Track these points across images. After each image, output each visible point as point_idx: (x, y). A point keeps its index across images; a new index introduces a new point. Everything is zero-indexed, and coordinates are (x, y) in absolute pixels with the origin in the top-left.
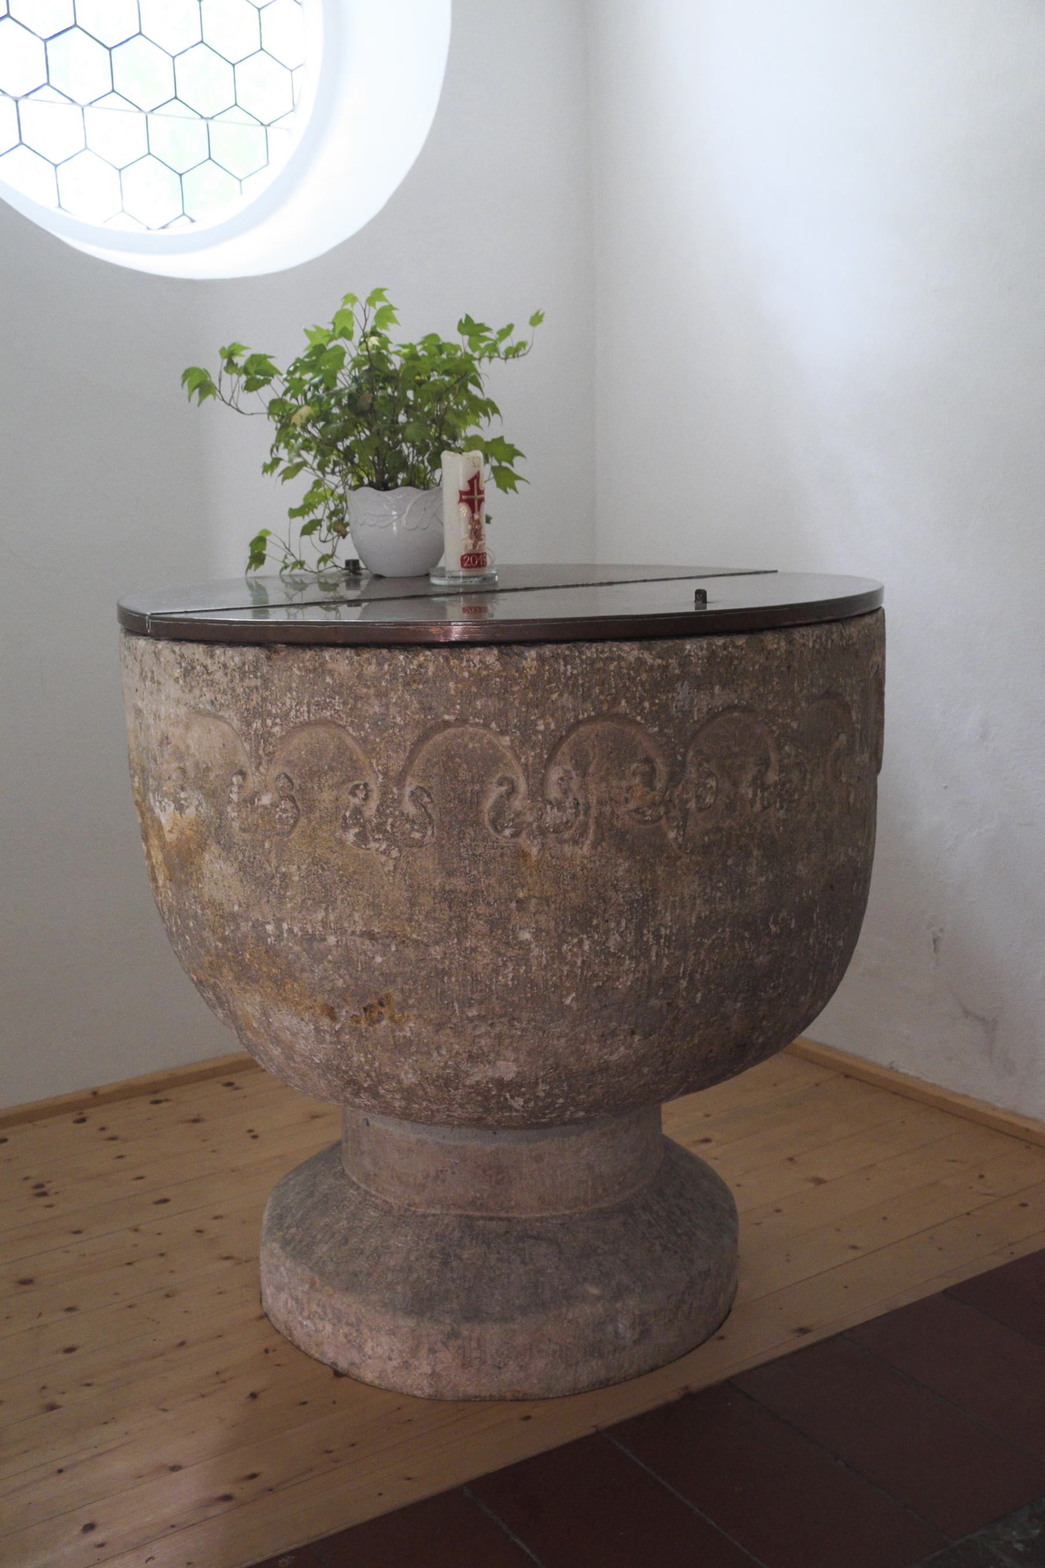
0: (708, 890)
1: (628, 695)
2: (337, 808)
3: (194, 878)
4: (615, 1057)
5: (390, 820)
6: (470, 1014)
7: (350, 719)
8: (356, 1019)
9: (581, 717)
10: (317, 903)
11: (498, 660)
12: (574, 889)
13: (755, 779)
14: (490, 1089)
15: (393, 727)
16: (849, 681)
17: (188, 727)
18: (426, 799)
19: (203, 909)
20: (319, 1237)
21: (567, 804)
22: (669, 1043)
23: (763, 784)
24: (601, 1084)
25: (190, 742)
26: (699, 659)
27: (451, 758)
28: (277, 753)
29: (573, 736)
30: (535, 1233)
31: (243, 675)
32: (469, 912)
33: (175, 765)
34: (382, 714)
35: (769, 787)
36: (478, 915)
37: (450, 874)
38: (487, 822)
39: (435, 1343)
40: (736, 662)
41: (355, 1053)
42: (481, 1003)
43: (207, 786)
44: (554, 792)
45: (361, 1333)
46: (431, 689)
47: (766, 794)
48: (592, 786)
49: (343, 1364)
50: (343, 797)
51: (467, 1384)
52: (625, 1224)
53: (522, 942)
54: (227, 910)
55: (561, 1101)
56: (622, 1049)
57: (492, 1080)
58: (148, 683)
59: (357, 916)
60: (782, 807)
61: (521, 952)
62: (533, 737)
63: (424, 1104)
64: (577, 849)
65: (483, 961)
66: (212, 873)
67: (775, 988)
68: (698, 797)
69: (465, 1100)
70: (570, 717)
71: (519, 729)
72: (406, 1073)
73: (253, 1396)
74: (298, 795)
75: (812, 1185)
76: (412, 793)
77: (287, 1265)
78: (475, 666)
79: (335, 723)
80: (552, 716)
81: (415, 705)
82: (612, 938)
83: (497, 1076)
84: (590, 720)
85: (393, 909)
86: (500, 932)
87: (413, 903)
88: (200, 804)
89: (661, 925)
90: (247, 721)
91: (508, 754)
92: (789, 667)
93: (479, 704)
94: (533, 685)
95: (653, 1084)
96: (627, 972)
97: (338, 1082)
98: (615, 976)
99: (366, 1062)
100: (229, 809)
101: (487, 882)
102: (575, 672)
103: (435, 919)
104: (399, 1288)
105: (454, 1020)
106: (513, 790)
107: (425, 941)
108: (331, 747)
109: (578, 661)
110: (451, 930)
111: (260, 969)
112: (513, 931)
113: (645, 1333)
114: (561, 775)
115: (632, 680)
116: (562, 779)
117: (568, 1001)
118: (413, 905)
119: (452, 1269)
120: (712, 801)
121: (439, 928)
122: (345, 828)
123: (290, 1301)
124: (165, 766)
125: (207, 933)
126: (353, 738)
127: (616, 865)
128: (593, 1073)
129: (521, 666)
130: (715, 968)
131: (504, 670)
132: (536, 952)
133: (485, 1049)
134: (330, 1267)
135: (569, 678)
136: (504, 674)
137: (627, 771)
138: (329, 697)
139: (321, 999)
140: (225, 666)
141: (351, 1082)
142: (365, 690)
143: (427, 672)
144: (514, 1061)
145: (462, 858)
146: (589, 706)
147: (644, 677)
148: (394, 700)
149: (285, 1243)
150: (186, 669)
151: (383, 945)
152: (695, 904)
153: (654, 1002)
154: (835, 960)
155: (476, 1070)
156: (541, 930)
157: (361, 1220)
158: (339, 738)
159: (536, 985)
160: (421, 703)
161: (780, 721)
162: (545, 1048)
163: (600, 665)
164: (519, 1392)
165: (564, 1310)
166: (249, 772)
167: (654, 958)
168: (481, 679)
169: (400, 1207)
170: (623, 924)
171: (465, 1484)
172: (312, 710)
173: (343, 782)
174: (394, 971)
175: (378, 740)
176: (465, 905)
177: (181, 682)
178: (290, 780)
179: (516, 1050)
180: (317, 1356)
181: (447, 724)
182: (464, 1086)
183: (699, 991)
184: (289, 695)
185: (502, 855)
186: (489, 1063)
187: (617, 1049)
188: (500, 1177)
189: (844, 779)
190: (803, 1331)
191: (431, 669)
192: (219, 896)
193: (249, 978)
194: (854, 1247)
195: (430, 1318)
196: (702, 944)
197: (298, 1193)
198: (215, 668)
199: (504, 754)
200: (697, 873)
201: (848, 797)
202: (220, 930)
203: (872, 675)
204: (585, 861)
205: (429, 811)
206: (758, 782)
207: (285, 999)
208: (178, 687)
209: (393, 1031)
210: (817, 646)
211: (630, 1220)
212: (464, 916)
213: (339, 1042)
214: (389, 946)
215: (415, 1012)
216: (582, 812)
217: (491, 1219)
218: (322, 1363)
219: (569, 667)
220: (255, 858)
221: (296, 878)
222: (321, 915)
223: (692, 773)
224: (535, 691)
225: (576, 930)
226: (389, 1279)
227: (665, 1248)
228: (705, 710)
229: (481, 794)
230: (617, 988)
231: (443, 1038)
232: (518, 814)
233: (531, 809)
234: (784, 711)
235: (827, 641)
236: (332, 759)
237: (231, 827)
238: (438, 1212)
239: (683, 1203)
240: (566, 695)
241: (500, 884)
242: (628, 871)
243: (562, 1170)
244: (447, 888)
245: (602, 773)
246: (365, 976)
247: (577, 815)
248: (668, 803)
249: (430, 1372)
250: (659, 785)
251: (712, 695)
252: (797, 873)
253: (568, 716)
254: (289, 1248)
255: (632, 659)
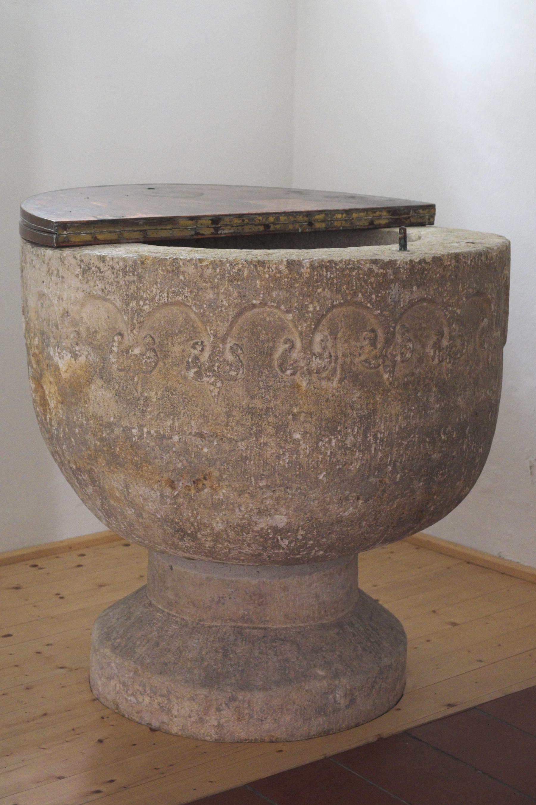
0: (406, 411)
1: (363, 290)
2: (183, 356)
3: (83, 401)
4: (347, 514)
5: (217, 364)
6: (261, 485)
7: (194, 302)
8: (188, 488)
9: (335, 303)
10: (168, 415)
11: (286, 268)
12: (327, 408)
13: (435, 344)
14: (269, 534)
15: (221, 307)
16: (490, 285)
17: (83, 305)
18: (240, 351)
19: (87, 420)
20: (138, 643)
21: (325, 356)
22: (379, 506)
23: (439, 347)
24: (336, 531)
25: (84, 315)
26: (405, 270)
27: (255, 326)
28: (145, 322)
29: (330, 315)
30: (282, 637)
31: (125, 273)
32: (263, 421)
33: (71, 329)
34: (214, 299)
35: (443, 349)
36: (269, 423)
37: (252, 398)
38: (276, 366)
39: (221, 705)
40: (426, 272)
41: (185, 511)
42: (268, 477)
43: (95, 343)
44: (317, 349)
45: (171, 701)
46: (245, 285)
47: (441, 353)
48: (339, 346)
49: (155, 724)
50: (187, 350)
51: (240, 731)
52: (338, 633)
53: (295, 439)
54: (106, 420)
55: (311, 542)
56: (351, 509)
57: (271, 527)
58: (54, 278)
59: (193, 423)
60: (450, 362)
61: (294, 446)
62: (306, 315)
63: (226, 544)
64: (330, 383)
65: (270, 451)
66: (96, 398)
67: (442, 475)
68: (402, 354)
69: (252, 541)
70: (329, 303)
71: (298, 310)
72: (217, 523)
73: (100, 741)
74: (158, 349)
75: (450, 626)
76: (231, 348)
77: (117, 661)
78: (273, 271)
79: (184, 304)
80: (318, 302)
81: (235, 294)
82: (349, 438)
83: (274, 525)
84: (341, 305)
85: (216, 419)
86: (282, 433)
87: (229, 415)
88: (89, 354)
89: (378, 431)
90: (126, 302)
91: (290, 325)
92: (456, 276)
93: (274, 294)
94: (307, 283)
95: (367, 533)
96: (357, 460)
97: (170, 531)
98: (349, 462)
99: (192, 516)
100: (111, 357)
101: (275, 403)
102: (332, 276)
103: (242, 425)
104: (196, 672)
105: (251, 488)
106: (293, 347)
107: (236, 438)
108: (181, 319)
109: (334, 269)
110: (252, 432)
111: (126, 458)
112: (290, 433)
113: (352, 701)
114: (322, 338)
115: (366, 281)
116: (322, 340)
117: (321, 477)
118: (228, 416)
119: (230, 659)
120: (410, 356)
121: (245, 431)
122: (188, 368)
123: (118, 685)
124: (65, 330)
125: (89, 436)
126: (195, 313)
127: (353, 394)
128: (332, 524)
129: (300, 272)
130: (409, 460)
131: (290, 274)
132: (303, 446)
133: (269, 507)
134: (148, 661)
135: (329, 280)
136: (290, 276)
137: (360, 337)
138: (182, 288)
139: (166, 476)
140: (113, 268)
141: (181, 530)
142: (204, 284)
143: (243, 274)
144: (286, 515)
145: (260, 388)
146: (340, 297)
147: (373, 280)
148: (222, 291)
149: (114, 648)
150: (84, 269)
151: (209, 441)
152: (398, 419)
153: (372, 479)
154: (477, 461)
155: (262, 521)
156: (307, 433)
157: (167, 631)
158: (186, 313)
159: (302, 467)
160: (239, 293)
161: (450, 309)
162: (305, 507)
163: (347, 272)
164: (273, 737)
165: (303, 683)
166: (126, 334)
167: (373, 452)
168: (276, 280)
169: (193, 622)
170: (356, 430)
171: (247, 784)
172: (170, 296)
173: (188, 340)
174: (215, 457)
175: (211, 315)
176: (261, 417)
177: (80, 277)
178: (153, 339)
179: (288, 508)
180: (137, 719)
181: (254, 306)
182: (253, 531)
183: (398, 473)
184: (155, 286)
185: (284, 387)
186: (270, 516)
187: (348, 509)
188: (261, 600)
189: (486, 346)
190: (450, 705)
191: (246, 273)
192: (100, 412)
193: (118, 463)
194: (481, 661)
195: (217, 689)
196: (401, 444)
197: (118, 619)
198: (106, 268)
199: (288, 325)
200: (400, 400)
201: (488, 358)
202: (99, 434)
203: (503, 282)
204: (334, 391)
205: (241, 358)
206: (437, 346)
207: (142, 476)
208: (78, 280)
209: (212, 495)
210: (473, 264)
211: (341, 631)
212: (260, 423)
213: (176, 503)
214: (213, 441)
215: (227, 483)
216: (333, 361)
217: (254, 628)
218: (141, 724)
219: (329, 273)
220: (127, 387)
221: (154, 400)
222: (169, 423)
223: (399, 339)
224: (308, 287)
225: (327, 433)
226: (189, 666)
227: (364, 649)
228: (407, 301)
229: (272, 350)
230: (351, 470)
231: (243, 500)
232: (295, 362)
233: (303, 359)
234: (453, 303)
235: (478, 261)
236: (181, 327)
237: (111, 368)
238: (219, 625)
239: (368, 629)
240: (326, 290)
241: (283, 404)
242: (360, 398)
243: (298, 598)
244: (250, 406)
245: (346, 338)
246: (196, 461)
247: (330, 362)
248: (384, 357)
249: (216, 724)
250: (379, 346)
251: (412, 292)
252: (458, 404)
253: (327, 302)
254: (117, 651)
255: (366, 269)
